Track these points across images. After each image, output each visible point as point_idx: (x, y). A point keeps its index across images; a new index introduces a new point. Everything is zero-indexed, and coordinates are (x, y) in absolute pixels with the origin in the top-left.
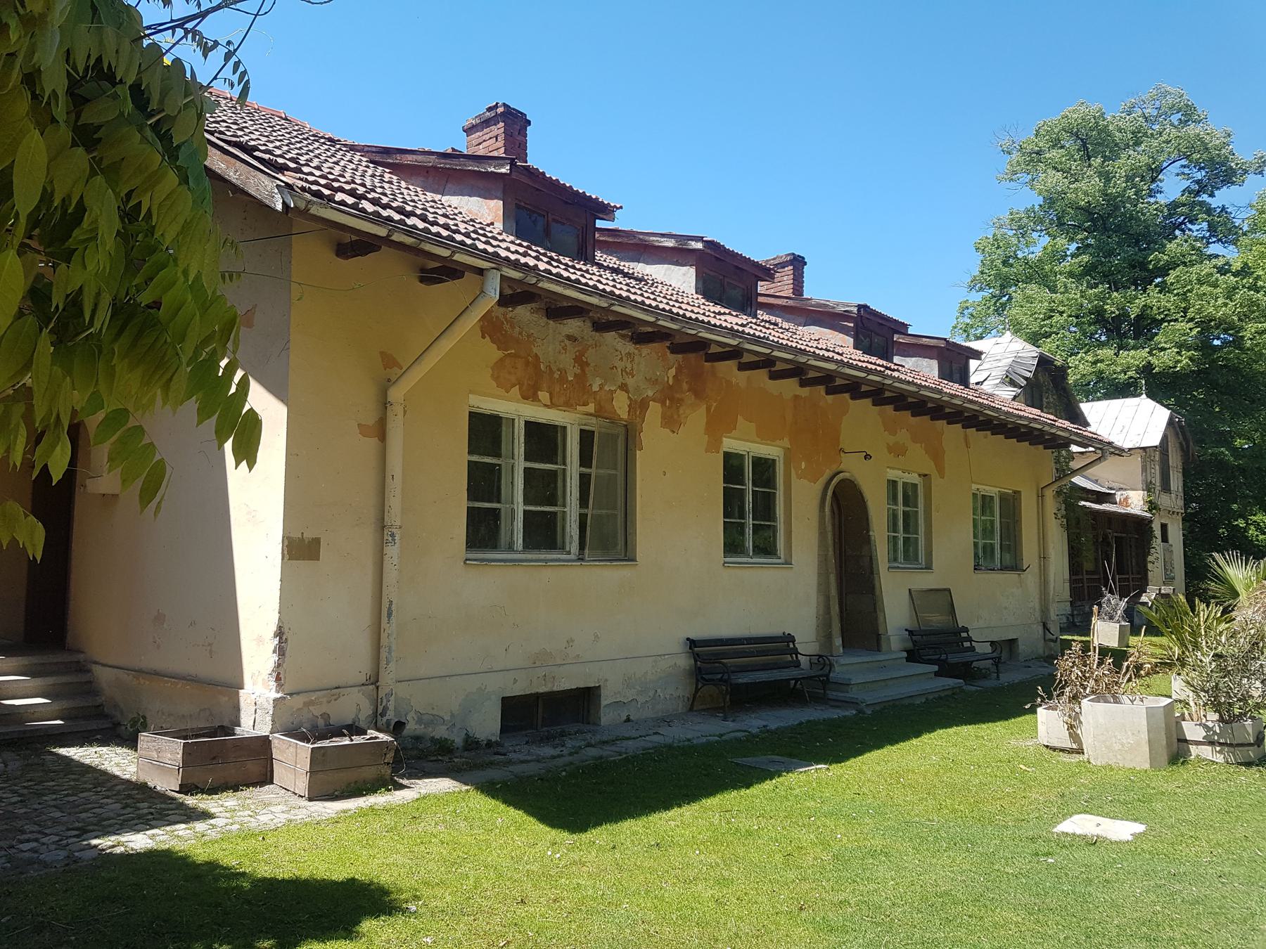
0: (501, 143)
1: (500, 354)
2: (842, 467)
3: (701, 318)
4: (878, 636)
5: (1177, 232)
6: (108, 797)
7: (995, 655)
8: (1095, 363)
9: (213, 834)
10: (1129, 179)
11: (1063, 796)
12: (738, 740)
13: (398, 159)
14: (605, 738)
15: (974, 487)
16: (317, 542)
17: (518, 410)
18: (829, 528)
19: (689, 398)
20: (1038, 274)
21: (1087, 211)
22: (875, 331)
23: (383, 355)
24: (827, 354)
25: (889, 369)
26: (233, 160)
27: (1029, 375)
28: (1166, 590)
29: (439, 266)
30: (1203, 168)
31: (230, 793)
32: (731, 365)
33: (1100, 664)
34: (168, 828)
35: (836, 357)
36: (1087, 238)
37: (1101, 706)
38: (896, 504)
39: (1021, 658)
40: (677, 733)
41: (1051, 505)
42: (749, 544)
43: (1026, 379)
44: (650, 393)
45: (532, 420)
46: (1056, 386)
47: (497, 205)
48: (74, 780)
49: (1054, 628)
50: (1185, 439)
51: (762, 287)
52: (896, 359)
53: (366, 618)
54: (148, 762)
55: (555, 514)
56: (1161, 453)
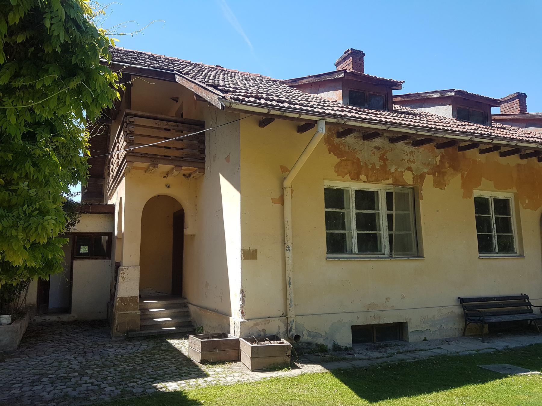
0: (351, 67)
1: (339, 160)
3: (506, 136)
9: (204, 385)
12: (489, 354)
14: (409, 349)
17: (350, 186)
23: (282, 167)
24: (531, 139)
31: (221, 365)
32: (475, 151)
34: (187, 381)
40: (452, 349)
44: (426, 170)
45: (359, 189)
47: (340, 92)
48: (166, 355)
53: (279, 285)
54: (188, 347)
55: (376, 234)
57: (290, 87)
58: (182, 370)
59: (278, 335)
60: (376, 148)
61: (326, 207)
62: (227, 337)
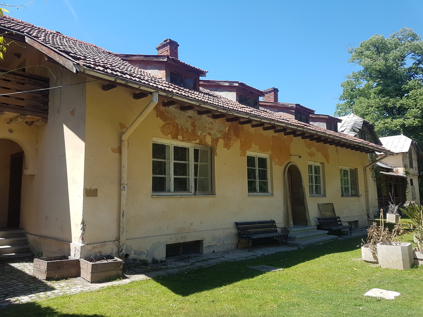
1: (164, 123)
2: (291, 161)
3: (268, 117)
4: (306, 221)
5: (412, 78)
6: (20, 282)
7: (349, 226)
8: (384, 124)
9: (53, 296)
10: (394, 60)
11: (369, 280)
12: (253, 259)
13: (131, 58)
14: (204, 259)
15: (340, 167)
16: (96, 190)
17: (171, 143)
18: (287, 182)
19: (234, 137)
20: (364, 94)
21: (380, 71)
22: (303, 113)
24: (282, 121)
25: (306, 126)
26: (61, 56)
27: (360, 128)
28: (412, 202)
29: (140, 94)
30: (420, 56)
32: (249, 125)
33: (384, 230)
34: (37, 294)
35: (287, 122)
36: (380, 81)
37: (384, 246)
38: (312, 173)
39: (360, 227)
40: (230, 257)
41: (370, 174)
42: (258, 188)
43: (359, 129)
44: (219, 136)
45: (176, 146)
46: (370, 132)
48: (12, 275)
49: (372, 217)
50: (418, 149)
51: (261, 99)
52: (311, 123)
53: (115, 216)
55: (186, 178)
56: (409, 154)
57: (124, 60)
58: (30, 286)
59: (111, 255)
60: (189, 117)
61: (153, 157)
62: (68, 259)
